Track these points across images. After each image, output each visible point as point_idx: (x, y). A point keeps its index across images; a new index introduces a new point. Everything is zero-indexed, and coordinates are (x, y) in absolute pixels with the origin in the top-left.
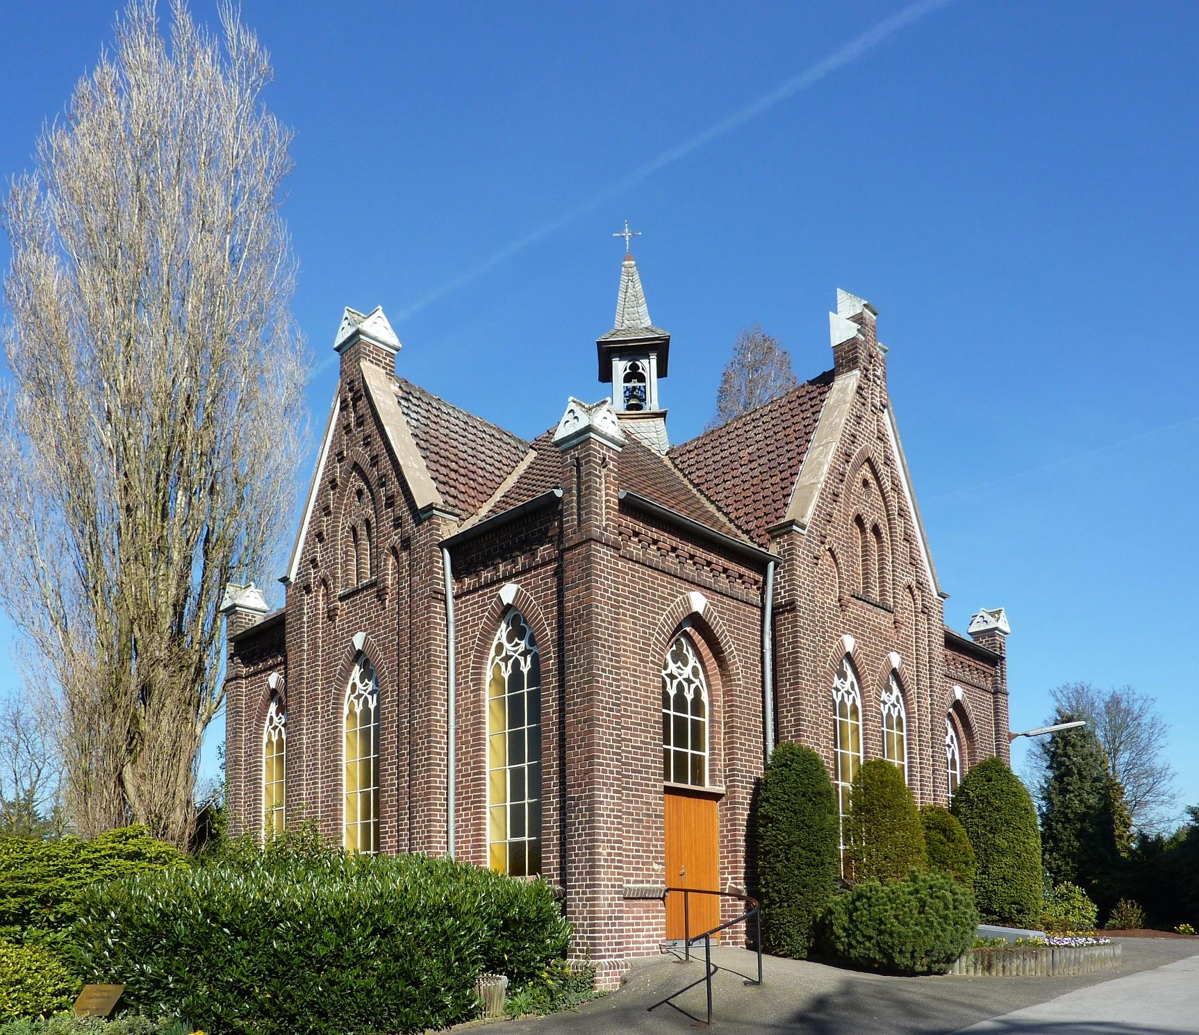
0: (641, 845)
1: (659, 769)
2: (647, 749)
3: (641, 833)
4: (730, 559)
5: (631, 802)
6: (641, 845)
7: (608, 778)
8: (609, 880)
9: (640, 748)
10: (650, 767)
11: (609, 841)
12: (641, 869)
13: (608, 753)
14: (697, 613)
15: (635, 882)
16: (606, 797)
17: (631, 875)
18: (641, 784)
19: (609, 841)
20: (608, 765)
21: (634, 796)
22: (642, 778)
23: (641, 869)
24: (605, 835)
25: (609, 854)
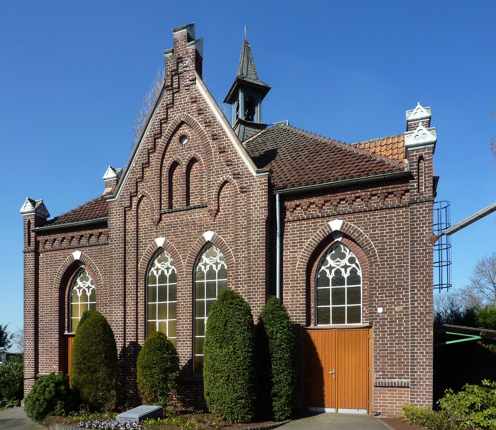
0: (48, 359)
1: (57, 329)
2: (51, 322)
3: (48, 354)
4: (92, 229)
5: (44, 343)
6: (48, 359)
7: (29, 336)
8: (29, 372)
9: (49, 322)
10: (53, 329)
11: (29, 358)
12: (48, 368)
13: (29, 327)
14: (77, 260)
15: (45, 372)
16: (28, 343)
17: (44, 370)
18: (48, 336)
19: (29, 358)
20: (29, 332)
21: (45, 341)
22: (49, 334)
23: (48, 368)
24: (28, 356)
25: (29, 363)
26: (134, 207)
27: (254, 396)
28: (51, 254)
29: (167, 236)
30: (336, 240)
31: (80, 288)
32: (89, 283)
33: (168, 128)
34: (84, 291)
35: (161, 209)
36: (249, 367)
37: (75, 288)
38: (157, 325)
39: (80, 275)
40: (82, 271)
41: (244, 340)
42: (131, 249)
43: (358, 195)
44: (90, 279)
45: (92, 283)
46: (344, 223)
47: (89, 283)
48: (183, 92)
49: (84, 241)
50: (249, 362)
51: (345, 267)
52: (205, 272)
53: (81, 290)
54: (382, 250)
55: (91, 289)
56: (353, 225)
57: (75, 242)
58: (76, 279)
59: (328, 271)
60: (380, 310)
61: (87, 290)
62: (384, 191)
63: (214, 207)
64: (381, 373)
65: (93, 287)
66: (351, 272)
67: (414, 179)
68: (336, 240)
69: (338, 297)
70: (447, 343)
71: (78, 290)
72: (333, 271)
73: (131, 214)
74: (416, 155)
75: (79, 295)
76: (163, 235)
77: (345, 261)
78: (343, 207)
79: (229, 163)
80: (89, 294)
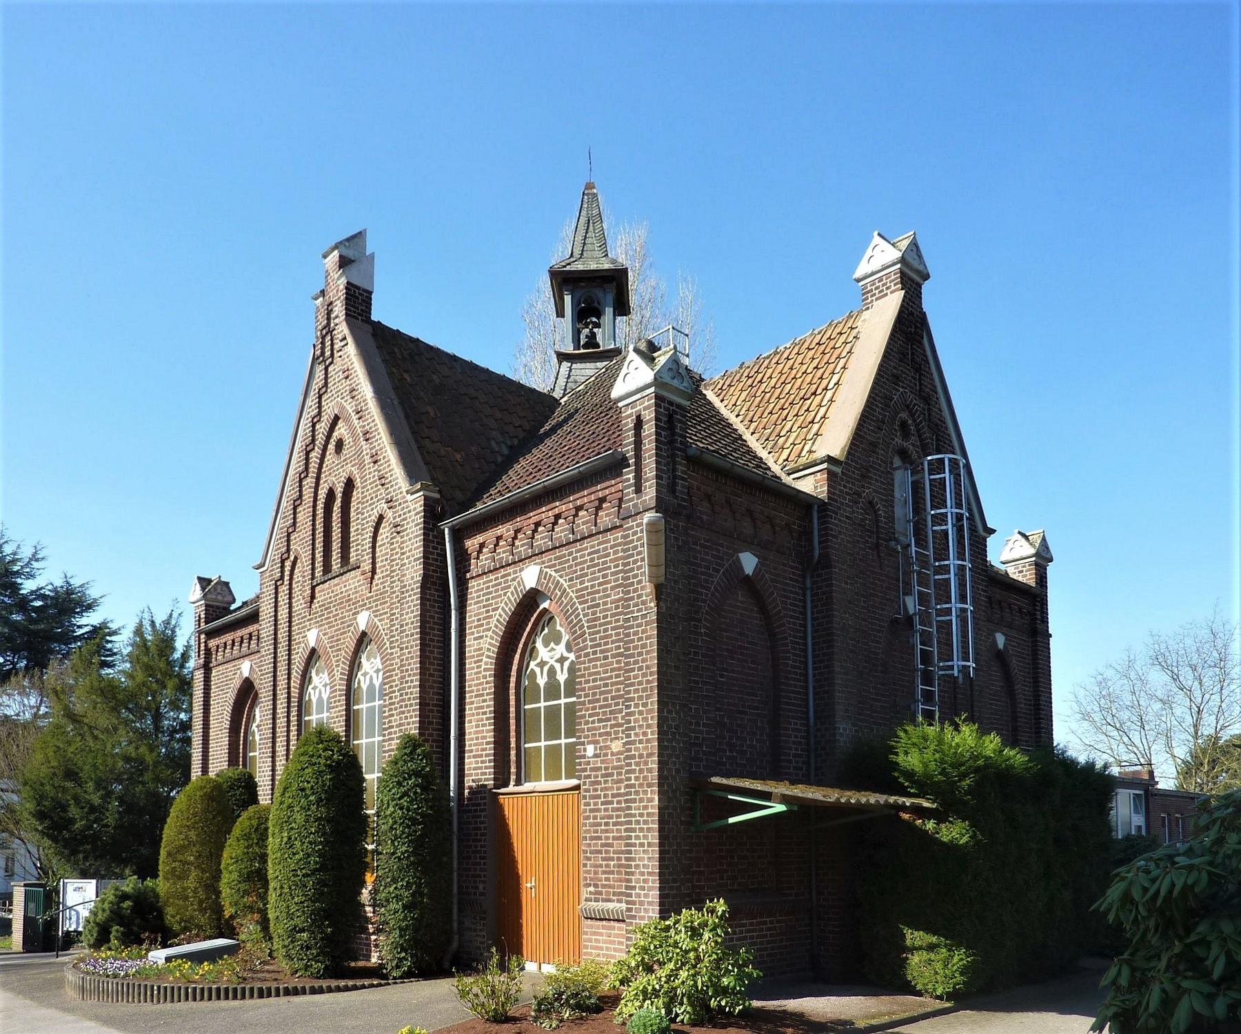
26: (287, 578)
27: (329, 926)
28: (496, 579)
30: (541, 607)
31: (542, 664)
32: (561, 649)
33: (322, 428)
34: (552, 672)
35: (313, 579)
36: (316, 870)
37: (532, 665)
39: (543, 630)
40: (546, 618)
41: (307, 821)
42: (283, 653)
43: (556, 511)
44: (565, 638)
45: (569, 648)
46: (541, 572)
47: (561, 649)
49: (541, 540)
50: (316, 863)
53: (546, 669)
55: (567, 664)
56: (553, 574)
57: (521, 547)
58: (534, 642)
61: (558, 666)
62: (593, 497)
63: (367, 566)
64: (592, 889)
65: (572, 656)
66: (569, 669)
67: (629, 466)
68: (541, 607)
70: (732, 820)
71: (538, 670)
73: (284, 589)
74: (631, 415)
75: (542, 681)
80: (562, 677)
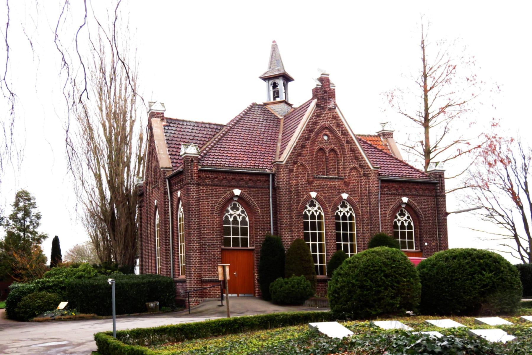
29: (318, 192)
38: (311, 245)
48: (327, 111)
51: (239, 215)
52: (309, 215)
54: (425, 215)
59: (229, 216)
60: (426, 244)
69: (403, 235)
72: (233, 217)
76: (315, 191)
77: (405, 218)
78: (242, 183)
79: (357, 158)
